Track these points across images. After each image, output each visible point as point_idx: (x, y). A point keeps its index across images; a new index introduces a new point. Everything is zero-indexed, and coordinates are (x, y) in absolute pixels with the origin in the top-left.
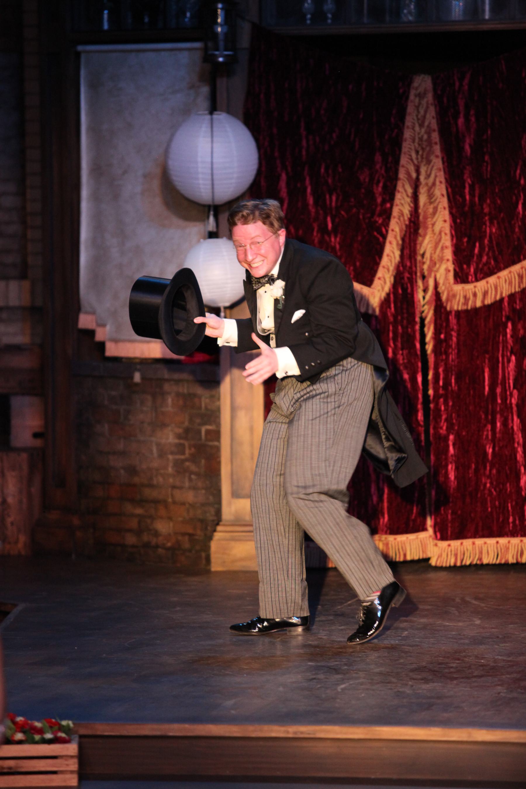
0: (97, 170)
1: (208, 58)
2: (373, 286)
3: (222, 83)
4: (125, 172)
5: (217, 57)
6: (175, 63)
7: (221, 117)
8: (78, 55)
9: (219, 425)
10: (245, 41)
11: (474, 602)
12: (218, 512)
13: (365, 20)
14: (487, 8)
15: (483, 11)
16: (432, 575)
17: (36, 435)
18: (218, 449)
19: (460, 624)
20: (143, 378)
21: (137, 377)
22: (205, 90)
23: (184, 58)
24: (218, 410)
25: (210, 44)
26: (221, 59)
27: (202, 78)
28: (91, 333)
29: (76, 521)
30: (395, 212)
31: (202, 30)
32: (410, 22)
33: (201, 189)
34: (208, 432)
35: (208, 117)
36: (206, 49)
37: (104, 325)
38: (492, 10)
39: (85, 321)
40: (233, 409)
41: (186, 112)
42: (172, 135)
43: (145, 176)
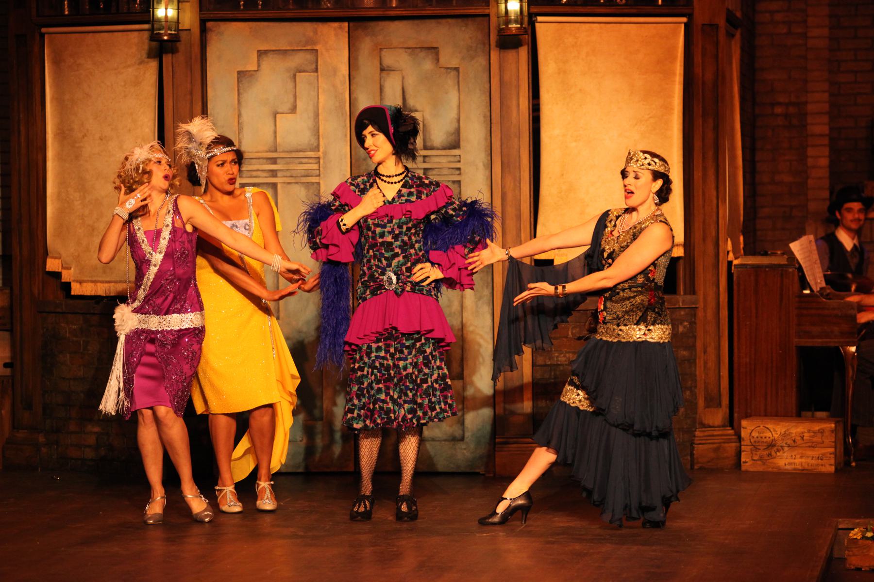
0: (63, 134)
3: (167, 59)
4: (85, 136)
8: (42, 36)
17: (6, 365)
23: (134, 37)
26: (165, 38)
27: (150, 55)
28: (58, 275)
29: (41, 439)
37: (69, 268)
39: (52, 265)
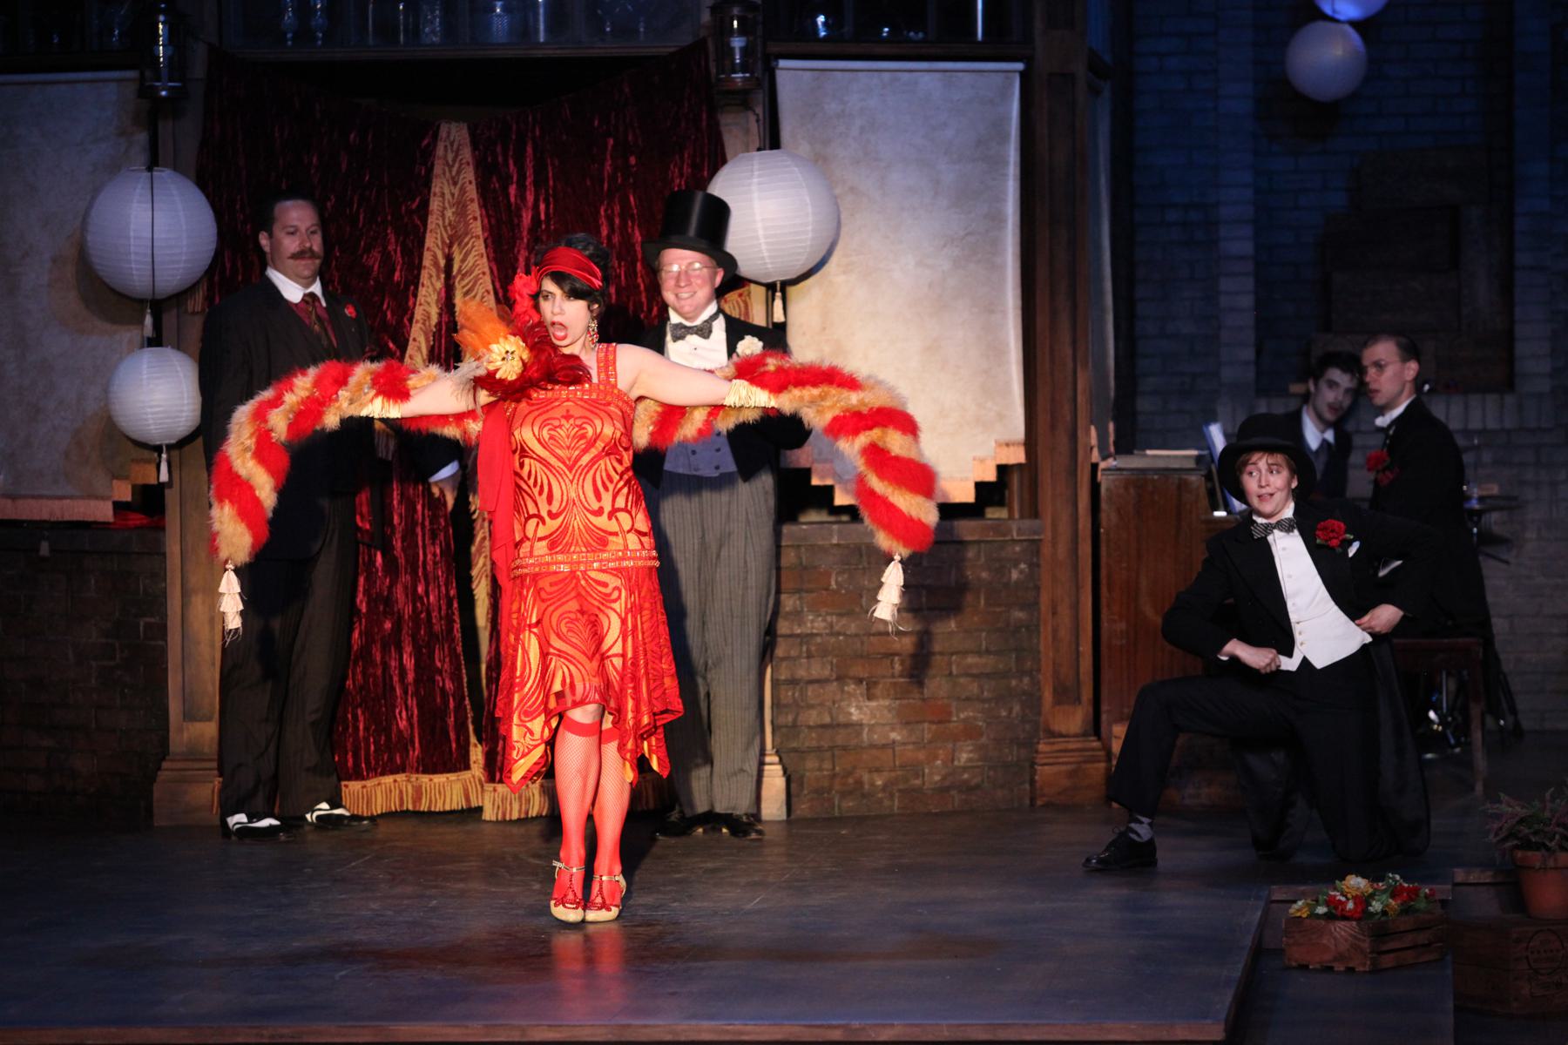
1: (146, 92)
2: (479, 488)
3: (165, 128)
5: (157, 90)
6: (102, 98)
7: (164, 175)
9: (164, 616)
10: (199, 70)
11: (532, 860)
12: (164, 742)
13: (371, 41)
14: (542, 27)
15: (537, 31)
16: (484, 826)
18: (163, 652)
19: (513, 890)
20: (52, 550)
21: (45, 548)
22: (142, 137)
24: (164, 593)
25: (148, 74)
30: (419, 313)
31: (137, 53)
32: (433, 44)
33: (136, 275)
34: (148, 626)
35: (147, 174)
36: (142, 78)
38: (548, 30)
40: (185, 594)
41: (114, 168)
42: (93, 198)
43: (54, 261)
